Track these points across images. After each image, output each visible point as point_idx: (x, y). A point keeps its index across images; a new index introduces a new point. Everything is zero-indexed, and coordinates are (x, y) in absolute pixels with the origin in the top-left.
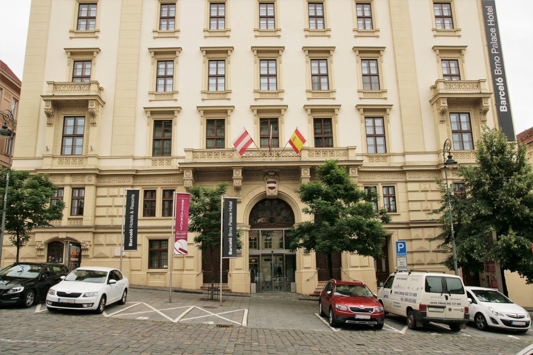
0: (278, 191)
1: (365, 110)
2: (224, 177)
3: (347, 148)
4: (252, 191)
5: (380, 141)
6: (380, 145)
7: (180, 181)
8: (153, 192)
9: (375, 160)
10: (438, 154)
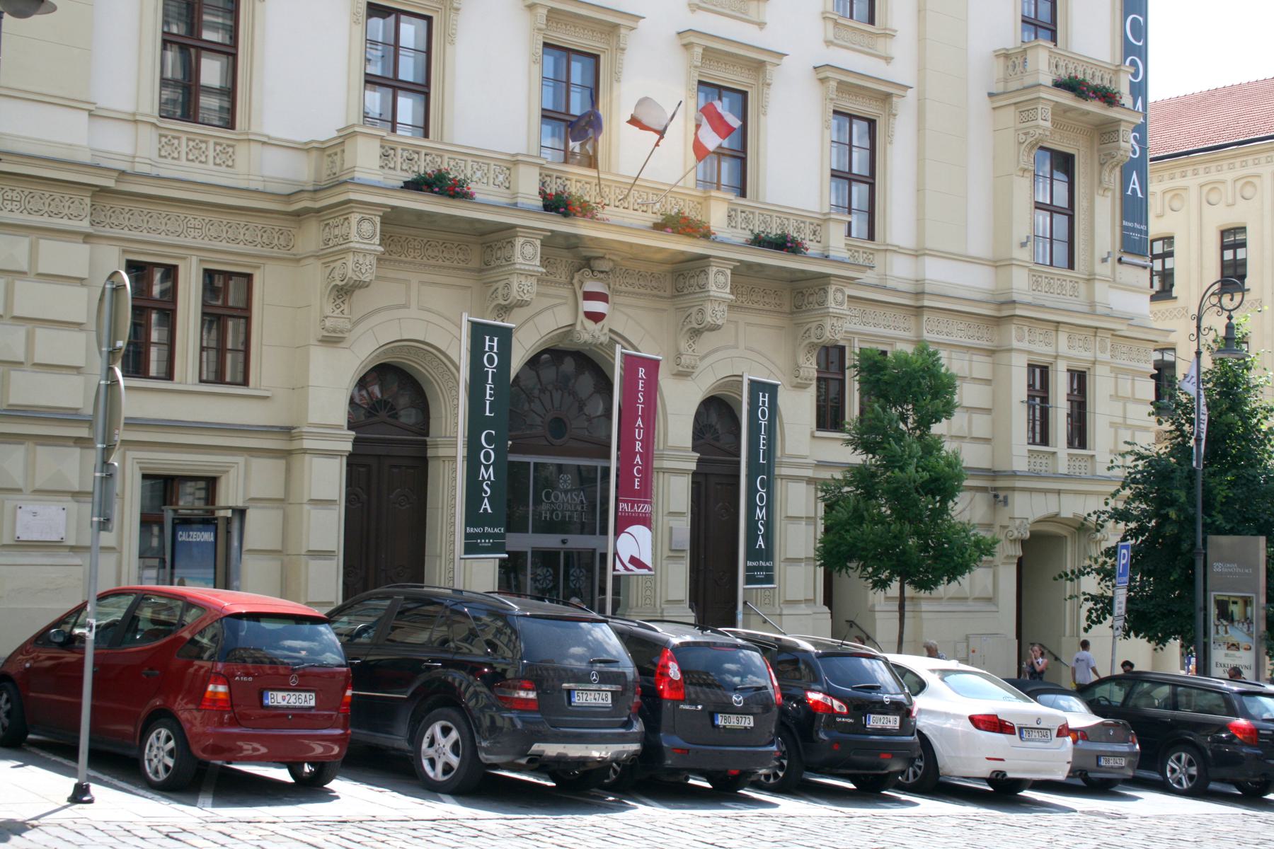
0: (611, 330)
1: (843, 87)
2: (766, 300)
3: (513, 155)
7: (241, 237)
9: (184, 149)
10: (996, 267)
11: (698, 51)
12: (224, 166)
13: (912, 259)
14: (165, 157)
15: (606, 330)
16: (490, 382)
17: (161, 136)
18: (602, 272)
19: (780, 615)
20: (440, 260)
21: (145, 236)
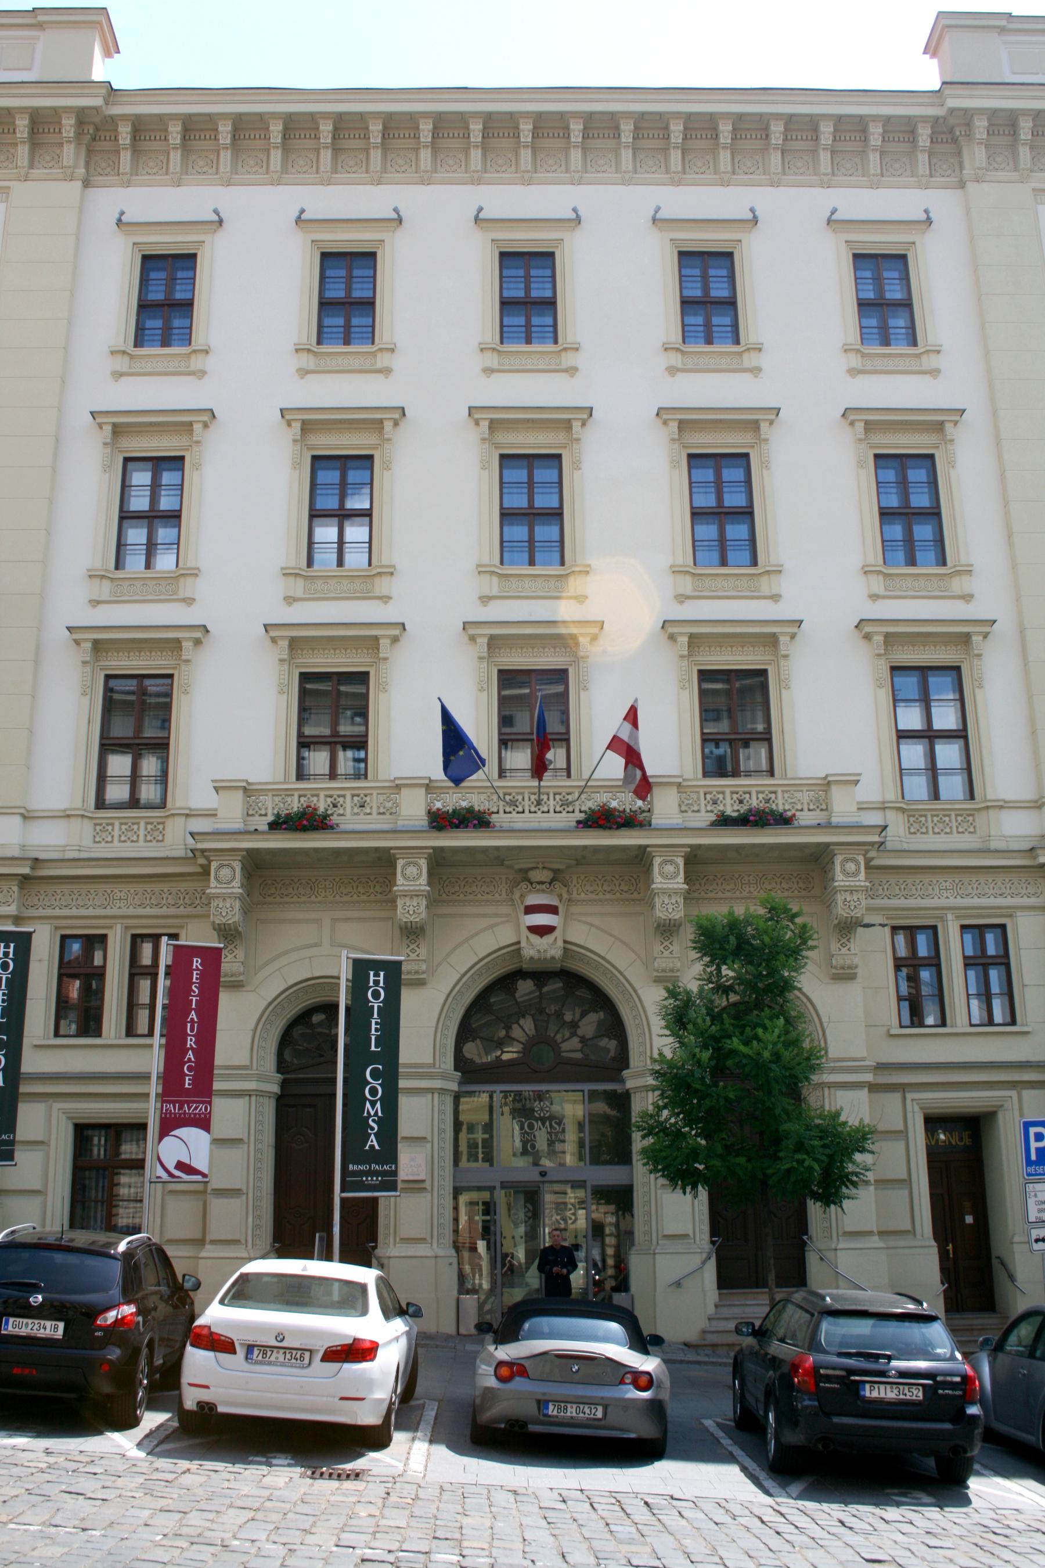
0: (565, 942)
1: (890, 639)
4: (467, 940)
5: (948, 754)
6: (950, 771)
8: (96, 941)
11: (879, 639)
12: (154, 841)
13: (1035, 812)
14: (99, 842)
15: (560, 943)
16: (375, 1016)
17: (96, 825)
18: (539, 883)
19: (836, 1250)
20: (355, 896)
21: (74, 912)
